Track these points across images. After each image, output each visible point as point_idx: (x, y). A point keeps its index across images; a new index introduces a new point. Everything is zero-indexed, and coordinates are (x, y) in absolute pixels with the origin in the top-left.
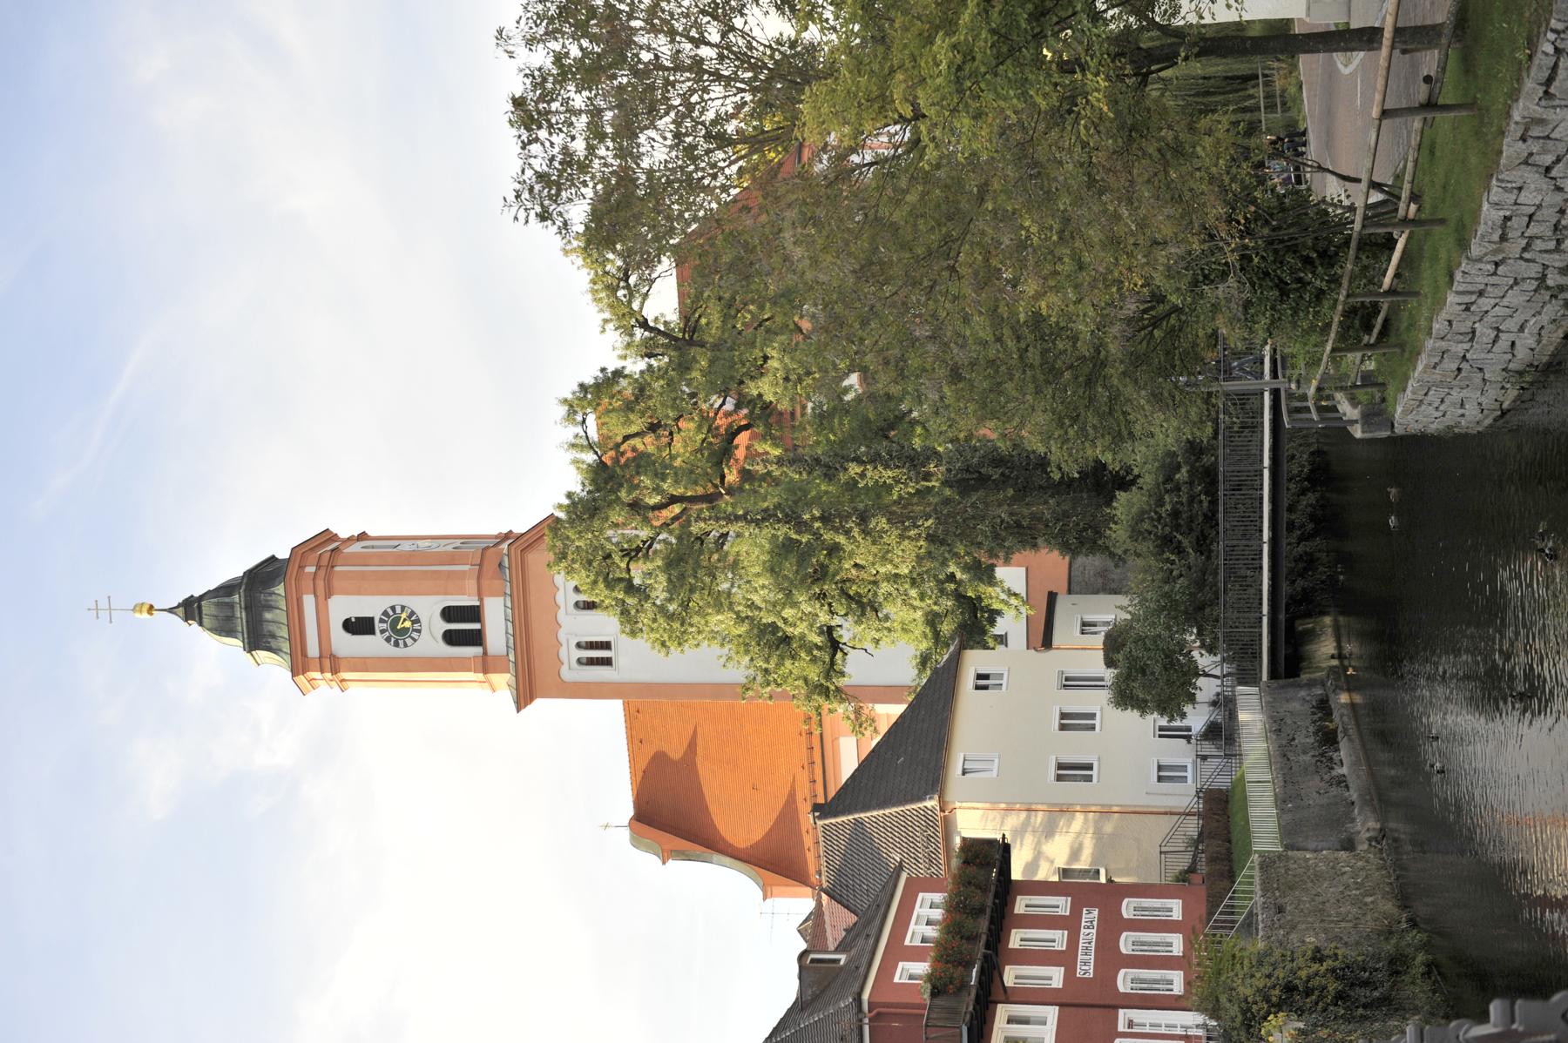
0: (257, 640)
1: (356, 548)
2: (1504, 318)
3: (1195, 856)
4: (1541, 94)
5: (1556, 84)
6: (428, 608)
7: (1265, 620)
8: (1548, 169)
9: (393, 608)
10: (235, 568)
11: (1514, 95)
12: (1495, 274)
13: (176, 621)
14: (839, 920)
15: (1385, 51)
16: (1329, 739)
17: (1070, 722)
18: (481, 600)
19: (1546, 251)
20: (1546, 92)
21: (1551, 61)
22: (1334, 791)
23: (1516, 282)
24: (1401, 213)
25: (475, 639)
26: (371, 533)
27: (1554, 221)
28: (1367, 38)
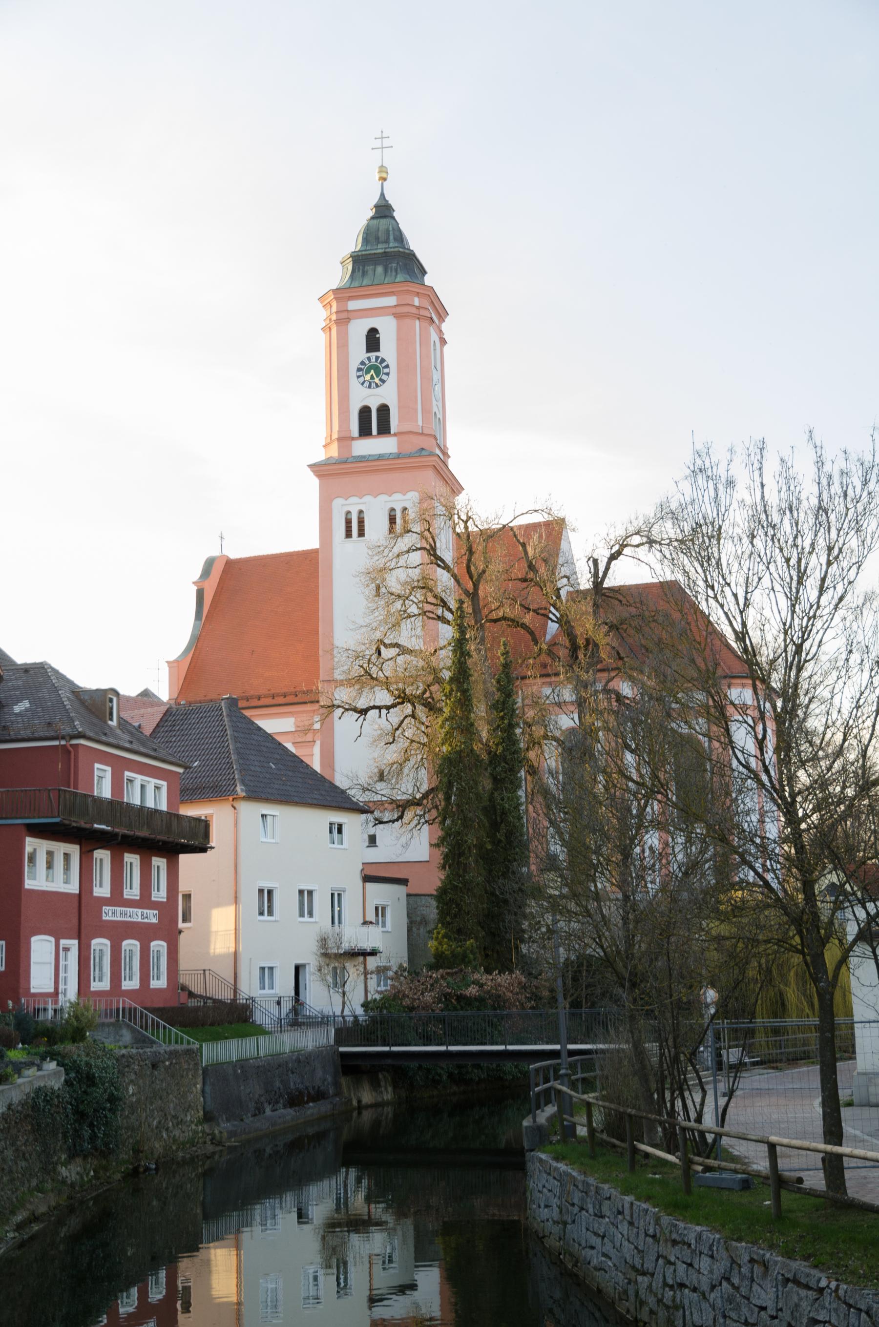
0: (361, 262)
1: (434, 337)
2: (612, 1242)
3: (201, 996)
4: (787, 1275)
5: (795, 1288)
6: (387, 394)
7: (386, 1049)
8: (728, 1280)
9: (387, 366)
10: (415, 244)
11: (789, 1254)
12: (646, 1235)
13: (375, 199)
14: (148, 722)
15: (822, 1146)
16: (295, 1100)
17: (306, 897)
18: (395, 435)
19: (664, 1276)
20: (788, 1280)
21: (812, 1284)
22: (252, 1105)
23: (639, 1251)
24: (697, 1159)
25: (365, 431)
26: (446, 348)
27: (688, 1283)
28: (833, 1131)
